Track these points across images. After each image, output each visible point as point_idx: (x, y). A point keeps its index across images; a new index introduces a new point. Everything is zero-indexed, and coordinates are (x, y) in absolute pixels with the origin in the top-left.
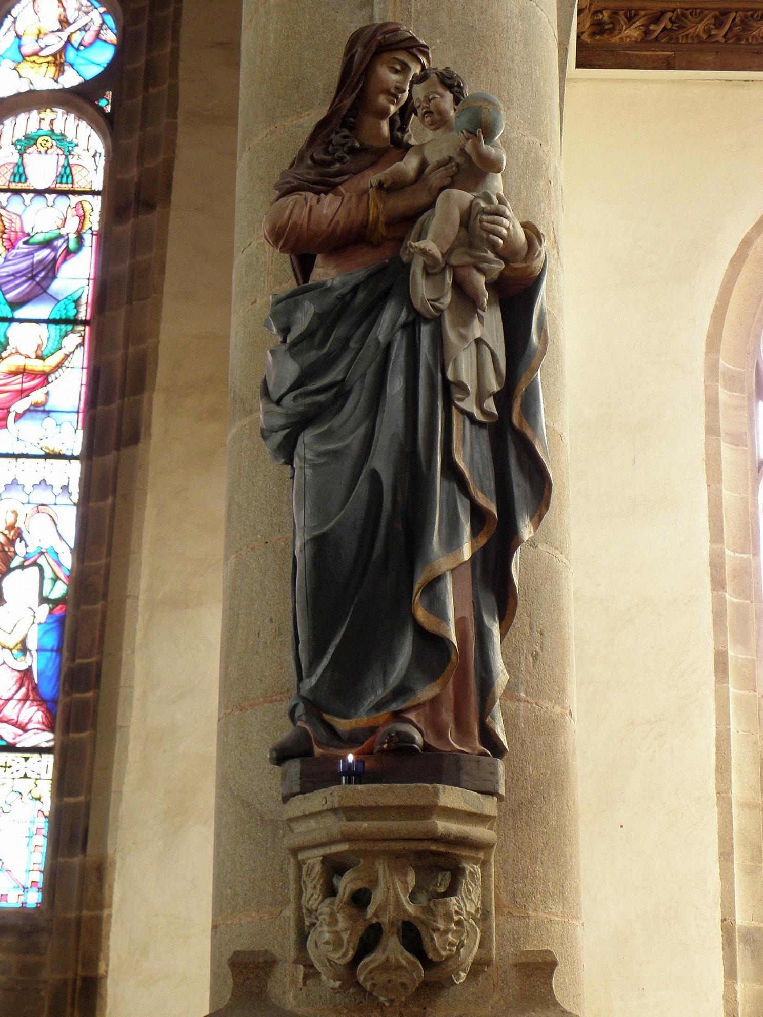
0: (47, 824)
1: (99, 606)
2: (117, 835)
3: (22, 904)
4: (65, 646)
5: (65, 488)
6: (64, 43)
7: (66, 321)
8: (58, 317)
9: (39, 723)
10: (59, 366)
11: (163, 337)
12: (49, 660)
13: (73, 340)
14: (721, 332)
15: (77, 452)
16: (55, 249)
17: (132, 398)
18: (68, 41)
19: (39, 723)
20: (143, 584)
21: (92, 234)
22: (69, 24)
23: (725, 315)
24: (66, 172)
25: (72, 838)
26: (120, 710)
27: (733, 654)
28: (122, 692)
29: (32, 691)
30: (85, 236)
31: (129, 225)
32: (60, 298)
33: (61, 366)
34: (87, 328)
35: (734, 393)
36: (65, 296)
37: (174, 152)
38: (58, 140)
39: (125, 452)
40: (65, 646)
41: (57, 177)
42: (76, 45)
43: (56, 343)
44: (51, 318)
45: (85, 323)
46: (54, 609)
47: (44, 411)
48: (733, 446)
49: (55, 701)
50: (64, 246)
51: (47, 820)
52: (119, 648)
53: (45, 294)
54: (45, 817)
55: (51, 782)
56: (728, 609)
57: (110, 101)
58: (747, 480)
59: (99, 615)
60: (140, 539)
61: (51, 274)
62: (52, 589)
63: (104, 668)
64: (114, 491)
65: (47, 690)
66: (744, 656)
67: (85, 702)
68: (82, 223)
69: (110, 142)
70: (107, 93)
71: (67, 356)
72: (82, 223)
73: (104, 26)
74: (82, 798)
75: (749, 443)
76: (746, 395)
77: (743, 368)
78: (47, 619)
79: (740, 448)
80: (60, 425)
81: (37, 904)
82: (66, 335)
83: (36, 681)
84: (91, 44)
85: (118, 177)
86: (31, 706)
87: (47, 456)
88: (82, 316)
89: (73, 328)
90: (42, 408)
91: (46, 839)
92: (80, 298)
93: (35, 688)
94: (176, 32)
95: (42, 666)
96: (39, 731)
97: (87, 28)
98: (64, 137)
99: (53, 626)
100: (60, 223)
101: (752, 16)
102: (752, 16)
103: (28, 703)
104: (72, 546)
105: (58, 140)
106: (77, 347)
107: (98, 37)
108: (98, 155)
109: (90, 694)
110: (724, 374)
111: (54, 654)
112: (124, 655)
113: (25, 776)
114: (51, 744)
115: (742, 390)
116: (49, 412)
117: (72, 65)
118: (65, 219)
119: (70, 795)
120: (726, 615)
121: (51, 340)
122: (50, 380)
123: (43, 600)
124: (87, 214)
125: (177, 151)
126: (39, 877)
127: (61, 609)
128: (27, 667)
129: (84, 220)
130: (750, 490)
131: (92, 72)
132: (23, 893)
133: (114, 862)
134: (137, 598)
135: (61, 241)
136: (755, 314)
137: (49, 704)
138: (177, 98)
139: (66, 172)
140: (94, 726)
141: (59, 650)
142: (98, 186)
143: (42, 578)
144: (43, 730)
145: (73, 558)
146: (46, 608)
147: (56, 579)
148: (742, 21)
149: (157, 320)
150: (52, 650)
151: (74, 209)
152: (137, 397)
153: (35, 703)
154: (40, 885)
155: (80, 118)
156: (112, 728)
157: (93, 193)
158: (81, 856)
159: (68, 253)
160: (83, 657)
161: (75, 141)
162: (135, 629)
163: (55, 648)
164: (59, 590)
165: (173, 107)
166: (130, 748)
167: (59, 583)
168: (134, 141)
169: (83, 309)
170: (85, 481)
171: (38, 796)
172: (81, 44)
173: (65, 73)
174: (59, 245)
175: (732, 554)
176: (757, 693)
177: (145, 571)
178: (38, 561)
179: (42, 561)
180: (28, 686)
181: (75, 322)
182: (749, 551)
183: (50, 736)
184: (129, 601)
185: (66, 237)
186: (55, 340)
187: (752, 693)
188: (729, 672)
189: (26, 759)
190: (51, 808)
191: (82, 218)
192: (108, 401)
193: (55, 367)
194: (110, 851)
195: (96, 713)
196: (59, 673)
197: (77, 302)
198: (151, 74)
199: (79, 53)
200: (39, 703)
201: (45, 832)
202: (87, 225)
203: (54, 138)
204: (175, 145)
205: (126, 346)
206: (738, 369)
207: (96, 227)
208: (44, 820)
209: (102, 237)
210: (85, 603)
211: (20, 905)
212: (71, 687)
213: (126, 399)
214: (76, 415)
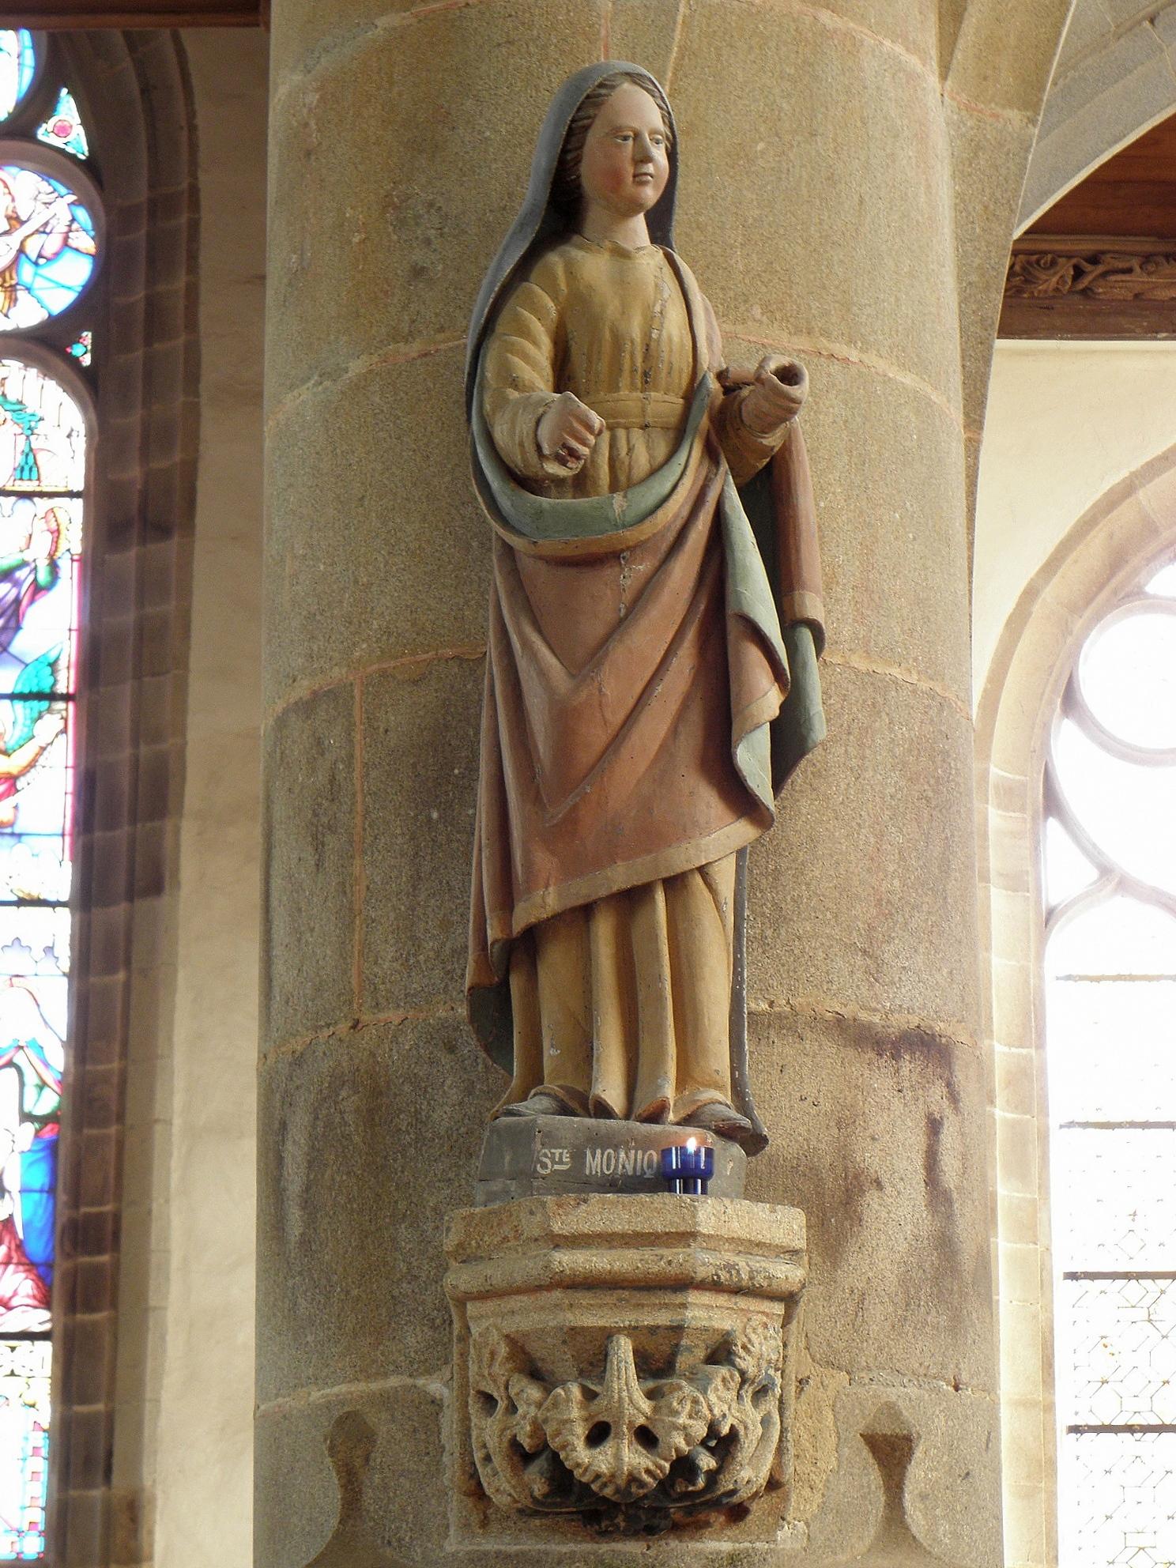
0: (48, 1441)
1: (113, 1130)
2: (155, 1460)
3: (18, 1554)
4: (60, 1186)
5: (49, 950)
6: (15, 252)
7: (39, 696)
8: (26, 691)
9: (28, 1296)
10: (32, 765)
11: (192, 735)
12: (37, 1204)
13: (51, 724)
14: (993, 729)
15: (65, 896)
16: (17, 584)
17: (149, 825)
18: (21, 251)
19: (28, 1296)
20: (178, 1101)
21: (72, 560)
22: (22, 223)
23: (998, 702)
24: (29, 465)
25: (88, 1462)
26: (152, 1284)
27: (1006, 1193)
28: (154, 1259)
29: (16, 1251)
30: (60, 563)
31: (133, 553)
32: (28, 660)
33: (35, 766)
34: (71, 706)
35: (1013, 814)
36: (35, 658)
37: (197, 451)
38: (14, 411)
39: (142, 905)
40: (60, 1186)
41: (15, 469)
42: (33, 257)
43: (26, 730)
44: (17, 691)
45: (67, 698)
46: (41, 1129)
47: (12, 834)
48: (1009, 892)
49: (49, 1265)
50: (31, 578)
51: (47, 1435)
52: (146, 1194)
53: (5, 654)
54: (44, 1431)
55: (50, 1381)
56: (998, 1132)
57: (89, 347)
58: (1029, 942)
59: (113, 1144)
60: (170, 1039)
61: (12, 624)
62: (38, 1100)
63: (125, 1223)
64: (128, 963)
65: (38, 1248)
66: (1021, 1195)
67: (98, 1269)
68: (56, 543)
69: (93, 417)
70: (84, 334)
71: (43, 749)
72: (56, 543)
73: (75, 226)
74: (100, 1407)
75: (1031, 886)
76: (1028, 816)
77: (1026, 776)
78: (33, 1145)
79: (1020, 893)
80: (37, 855)
81: (39, 1553)
82: (40, 717)
83: (21, 1236)
84: (57, 254)
85: (109, 476)
86: (16, 1272)
87: (21, 902)
88: (61, 689)
89: (49, 707)
90: (8, 830)
91: (47, 1462)
92: (56, 661)
93: (20, 1246)
94: (193, 257)
95: (27, 1215)
96: (29, 1308)
97: (48, 230)
98: (22, 407)
99: (41, 1155)
100: (23, 543)
101: (1038, 262)
102: (1038, 262)
103: (11, 1268)
104: (64, 1038)
105: (14, 411)
106: (57, 736)
107: (66, 244)
108: (74, 434)
109: (105, 1258)
110: (997, 787)
111: (45, 1195)
112: (155, 1206)
113: (12, 1374)
114: (47, 1327)
115: (1023, 809)
116: (20, 835)
117: (28, 289)
118: (31, 536)
119: (83, 1400)
120: (994, 1140)
121: (19, 726)
122: (19, 787)
123: (26, 1117)
124: (62, 528)
125: (202, 448)
126: (39, 1517)
127: (52, 1130)
128: (7, 1216)
129: (58, 537)
130: (1033, 954)
131: (60, 301)
132: (17, 1539)
133: (153, 1500)
134: (169, 1123)
135: (26, 570)
136: (1043, 694)
137: (41, 1269)
138: (198, 365)
139: (29, 465)
140: (114, 1305)
141: (51, 1190)
142: (79, 485)
143: (22, 1084)
144: (35, 1307)
145: (67, 1055)
146: (30, 1128)
147: (43, 1085)
148: (1023, 268)
149: (181, 709)
150: (41, 1191)
151: (44, 520)
152: (157, 824)
153: (21, 1268)
154: (41, 1527)
155: (45, 375)
156: (142, 1309)
157: (71, 495)
158: (103, 1489)
159: (37, 590)
160: (92, 1204)
161: (39, 414)
162: (169, 1168)
163: (46, 1188)
164: (47, 1102)
165: (193, 378)
166: (168, 1338)
167: (46, 1091)
168: (136, 418)
169: (62, 676)
170: (81, 939)
171: (31, 1402)
172: (40, 256)
173: (18, 303)
174: (23, 578)
175: (1006, 1049)
176: (1038, 1247)
177: (179, 1083)
178: (15, 1060)
179: (19, 1059)
180: (10, 1243)
181: (52, 697)
182: (1031, 1043)
183: (46, 1315)
184: (158, 1128)
185: (33, 565)
186: (24, 725)
187: (1032, 1246)
188: (999, 1219)
189: (13, 1349)
190: (53, 1418)
191: (56, 534)
192: (111, 824)
193: (26, 767)
194: (147, 1482)
195: (115, 1287)
196: (54, 1224)
197: (53, 666)
198: (156, 321)
199: (41, 271)
200: (27, 1267)
201: (45, 1452)
202: (63, 545)
203: (8, 407)
204: (198, 437)
205: (135, 742)
206: (1018, 777)
207: (77, 549)
208: (43, 1435)
209: (89, 565)
210: (91, 1125)
211: (13, 1556)
212: (75, 1244)
213: (139, 826)
214: (61, 838)
